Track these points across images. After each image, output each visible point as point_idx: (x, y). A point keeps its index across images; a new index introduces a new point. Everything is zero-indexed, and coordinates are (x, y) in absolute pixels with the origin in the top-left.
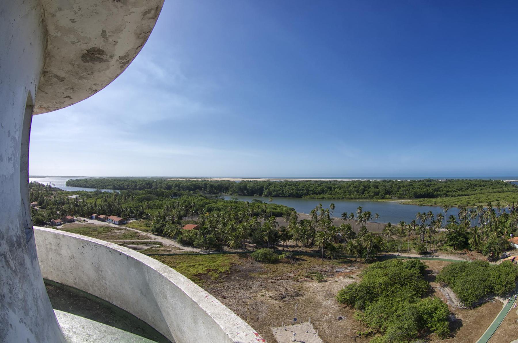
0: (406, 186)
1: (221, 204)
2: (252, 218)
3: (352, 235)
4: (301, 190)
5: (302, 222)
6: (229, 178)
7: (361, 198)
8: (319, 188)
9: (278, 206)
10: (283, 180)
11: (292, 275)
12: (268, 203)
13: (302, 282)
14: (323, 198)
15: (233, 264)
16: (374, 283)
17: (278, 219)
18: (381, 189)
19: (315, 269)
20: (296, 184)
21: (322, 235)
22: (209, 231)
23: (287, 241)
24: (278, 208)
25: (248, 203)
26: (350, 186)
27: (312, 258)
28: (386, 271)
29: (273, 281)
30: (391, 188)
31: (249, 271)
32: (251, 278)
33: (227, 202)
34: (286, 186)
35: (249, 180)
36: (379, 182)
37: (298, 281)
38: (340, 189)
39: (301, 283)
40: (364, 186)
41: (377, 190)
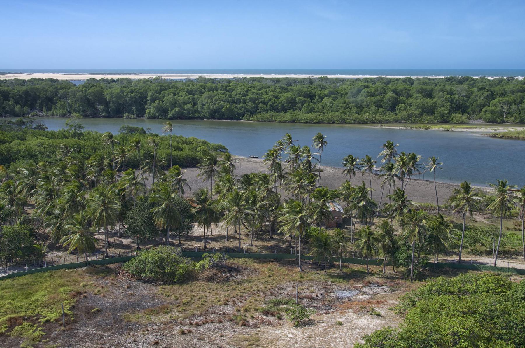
0: (513, 92)
1: (38, 141)
2: (123, 174)
3: (368, 211)
4: (238, 102)
5: (247, 180)
6: (54, 72)
7: (388, 122)
8: (284, 97)
9: (185, 142)
10: (194, 77)
11: (230, 310)
12: (161, 135)
13: (255, 326)
14: (294, 121)
15: (81, 294)
16: (437, 332)
17: (187, 173)
18: (439, 98)
19: (285, 292)
20: (227, 86)
21: (295, 211)
22: (9, 214)
23: (213, 225)
24: (186, 147)
25: (111, 136)
26: (359, 91)
27: (270, 265)
28: (468, 301)
29: (185, 328)
30: (468, 97)
31: (124, 308)
32: (130, 328)
33: (53, 136)
34: (201, 93)
35: (109, 77)
36: (436, 83)
37: (245, 324)
38: (335, 99)
39: (255, 331)
40: (395, 91)
41: (430, 101)
